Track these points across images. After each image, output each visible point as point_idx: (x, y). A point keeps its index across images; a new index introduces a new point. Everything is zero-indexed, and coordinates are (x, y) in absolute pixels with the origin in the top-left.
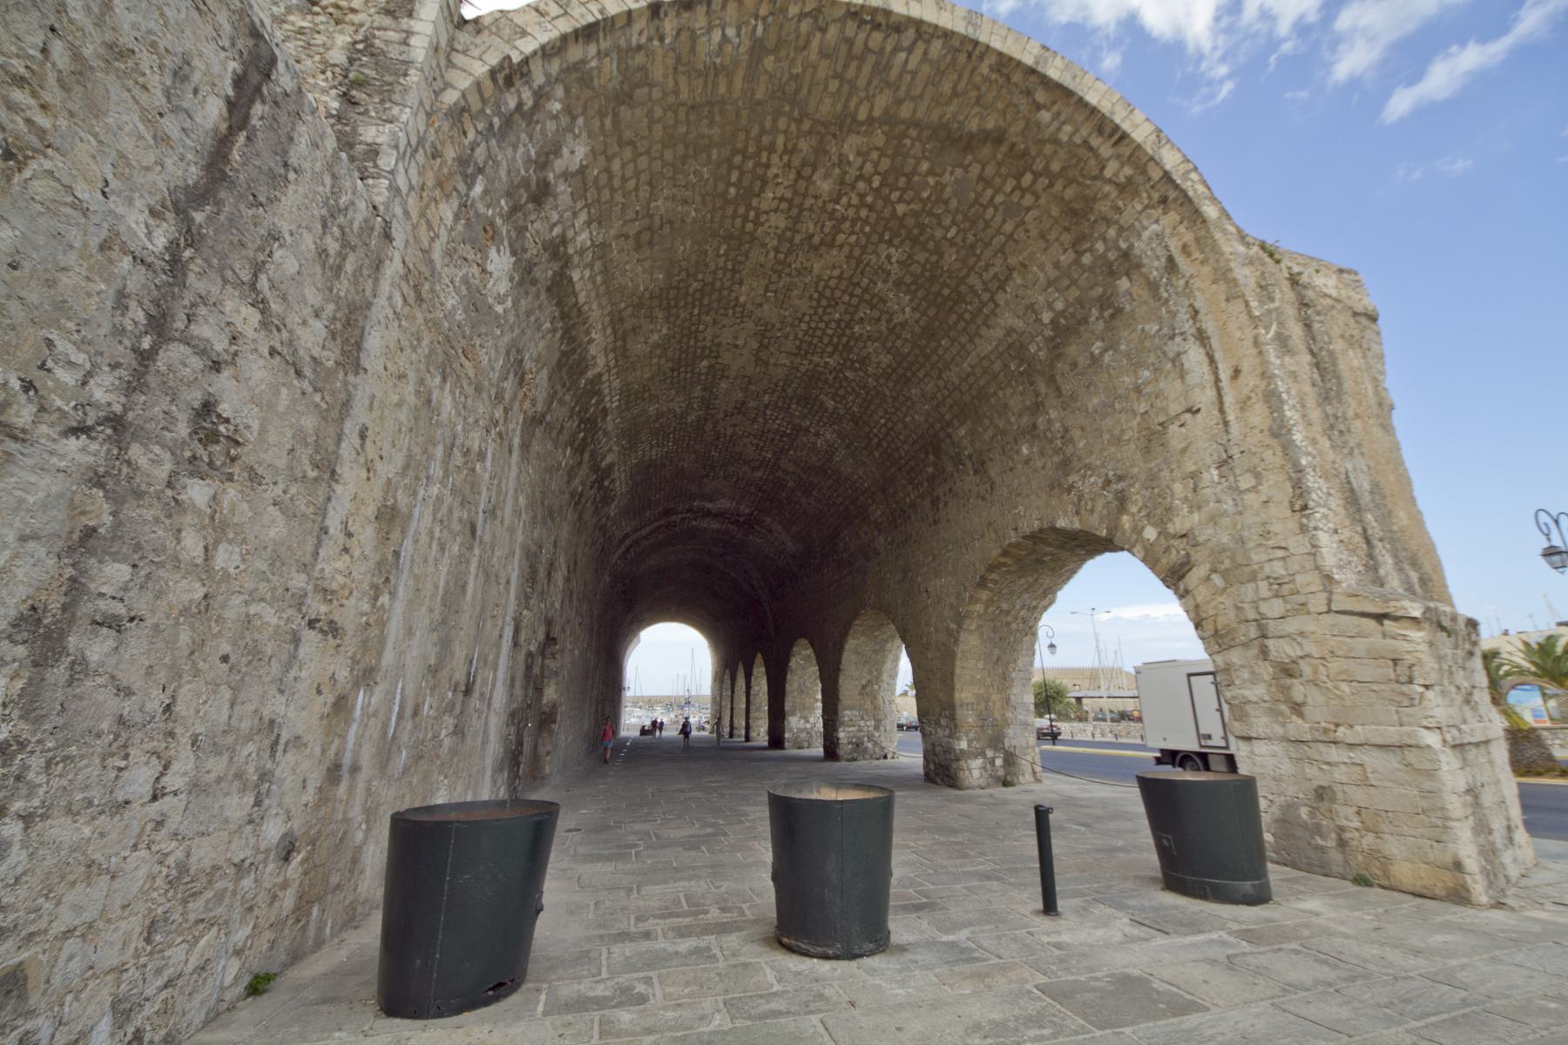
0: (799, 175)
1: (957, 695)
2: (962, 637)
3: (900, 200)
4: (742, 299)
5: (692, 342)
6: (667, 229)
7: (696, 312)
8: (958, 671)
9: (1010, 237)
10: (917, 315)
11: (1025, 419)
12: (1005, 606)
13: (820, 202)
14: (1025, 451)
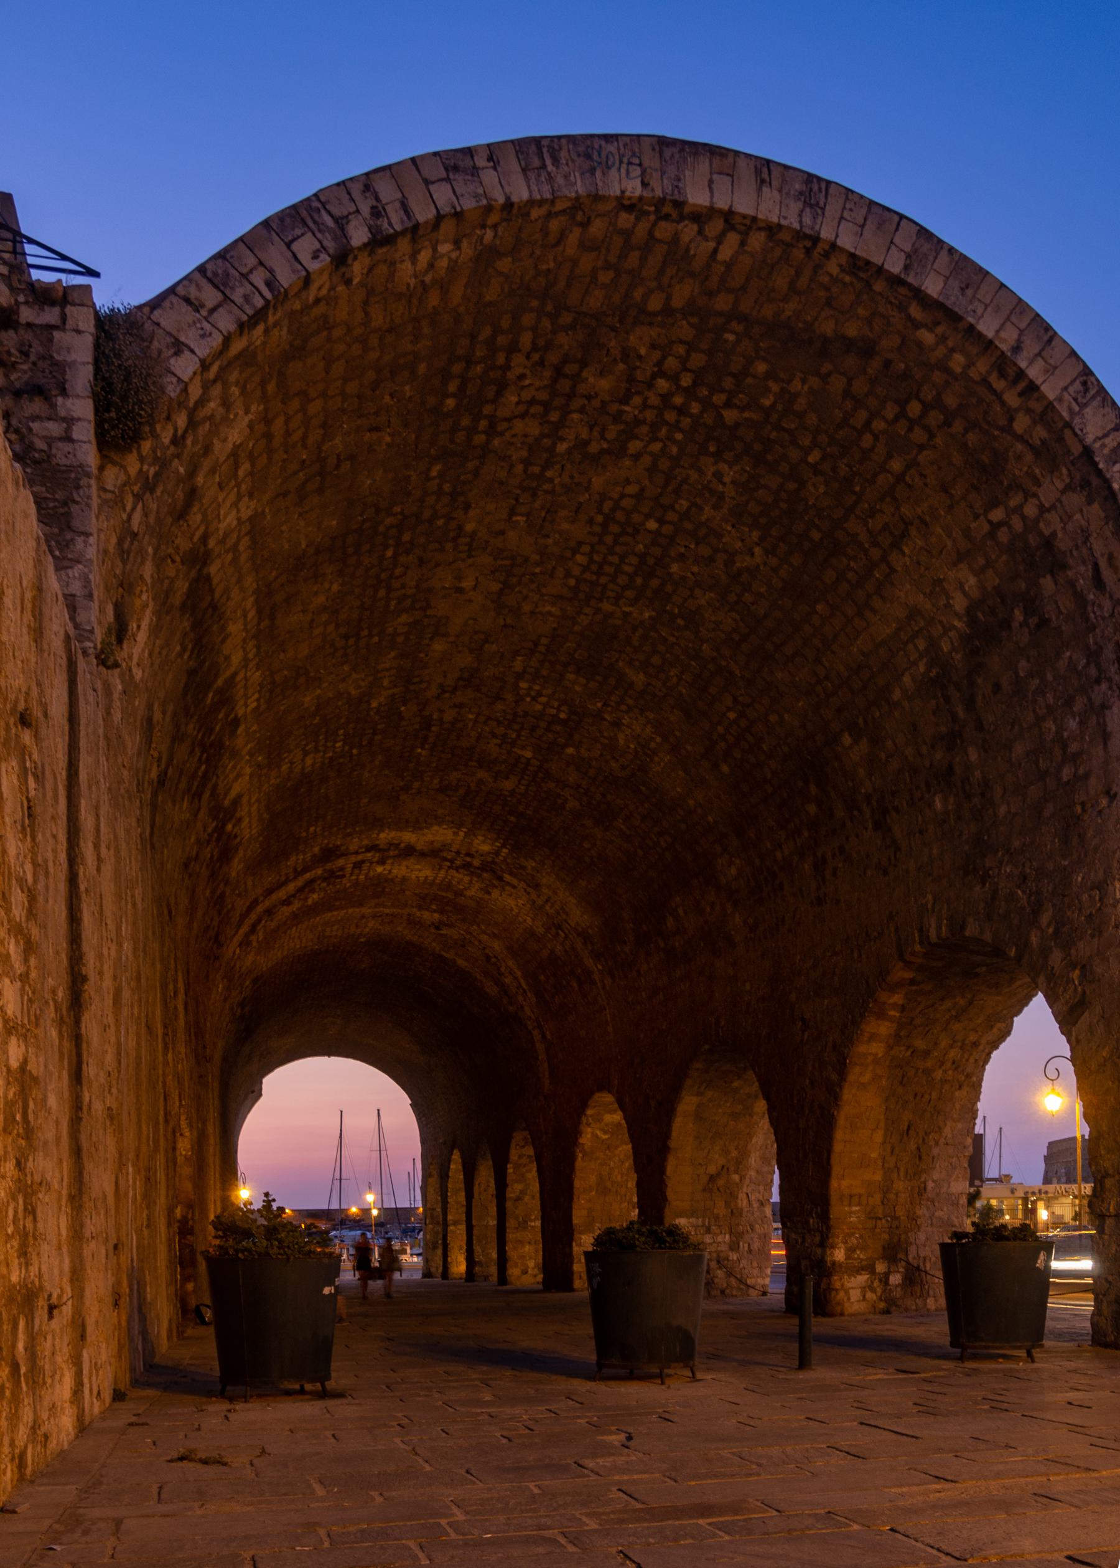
0: (558, 371)
1: (834, 1183)
2: (847, 1094)
3: (728, 404)
4: (469, 527)
5: (382, 593)
6: (346, 466)
7: (389, 553)
8: (838, 1147)
9: (900, 478)
10: (773, 561)
11: (939, 755)
12: (920, 1044)
13: (596, 403)
14: (938, 804)
